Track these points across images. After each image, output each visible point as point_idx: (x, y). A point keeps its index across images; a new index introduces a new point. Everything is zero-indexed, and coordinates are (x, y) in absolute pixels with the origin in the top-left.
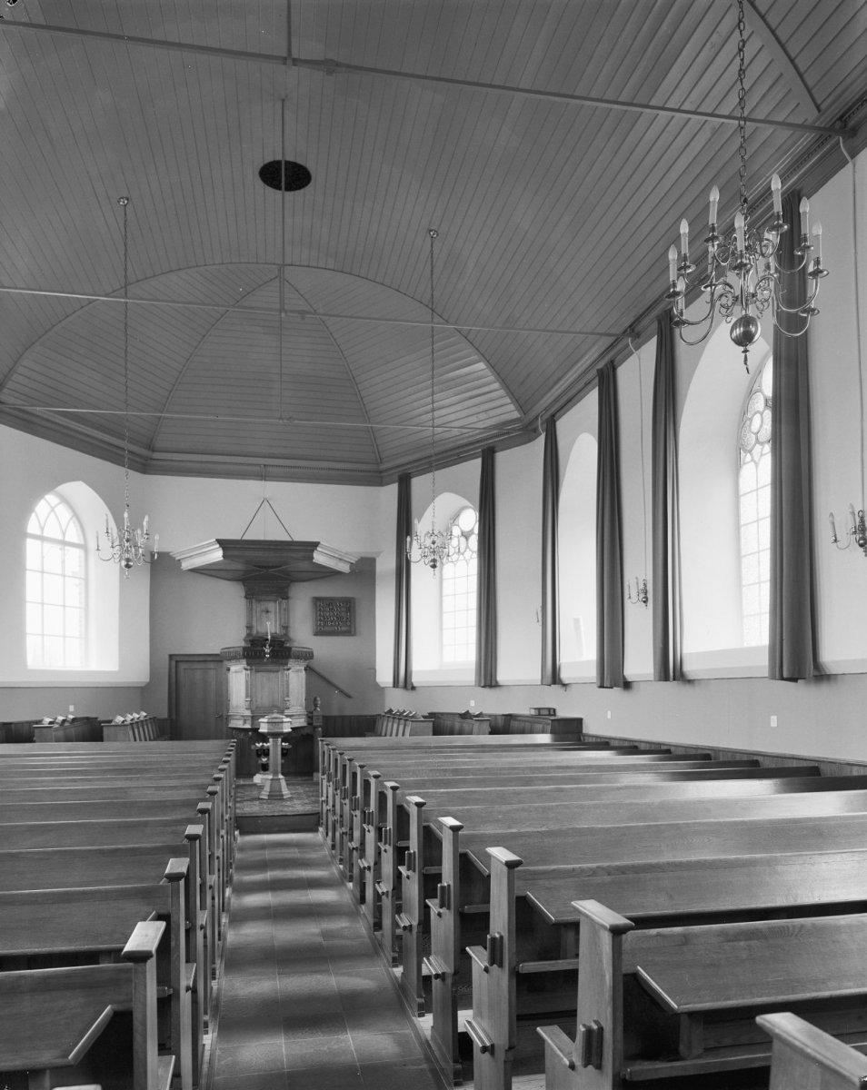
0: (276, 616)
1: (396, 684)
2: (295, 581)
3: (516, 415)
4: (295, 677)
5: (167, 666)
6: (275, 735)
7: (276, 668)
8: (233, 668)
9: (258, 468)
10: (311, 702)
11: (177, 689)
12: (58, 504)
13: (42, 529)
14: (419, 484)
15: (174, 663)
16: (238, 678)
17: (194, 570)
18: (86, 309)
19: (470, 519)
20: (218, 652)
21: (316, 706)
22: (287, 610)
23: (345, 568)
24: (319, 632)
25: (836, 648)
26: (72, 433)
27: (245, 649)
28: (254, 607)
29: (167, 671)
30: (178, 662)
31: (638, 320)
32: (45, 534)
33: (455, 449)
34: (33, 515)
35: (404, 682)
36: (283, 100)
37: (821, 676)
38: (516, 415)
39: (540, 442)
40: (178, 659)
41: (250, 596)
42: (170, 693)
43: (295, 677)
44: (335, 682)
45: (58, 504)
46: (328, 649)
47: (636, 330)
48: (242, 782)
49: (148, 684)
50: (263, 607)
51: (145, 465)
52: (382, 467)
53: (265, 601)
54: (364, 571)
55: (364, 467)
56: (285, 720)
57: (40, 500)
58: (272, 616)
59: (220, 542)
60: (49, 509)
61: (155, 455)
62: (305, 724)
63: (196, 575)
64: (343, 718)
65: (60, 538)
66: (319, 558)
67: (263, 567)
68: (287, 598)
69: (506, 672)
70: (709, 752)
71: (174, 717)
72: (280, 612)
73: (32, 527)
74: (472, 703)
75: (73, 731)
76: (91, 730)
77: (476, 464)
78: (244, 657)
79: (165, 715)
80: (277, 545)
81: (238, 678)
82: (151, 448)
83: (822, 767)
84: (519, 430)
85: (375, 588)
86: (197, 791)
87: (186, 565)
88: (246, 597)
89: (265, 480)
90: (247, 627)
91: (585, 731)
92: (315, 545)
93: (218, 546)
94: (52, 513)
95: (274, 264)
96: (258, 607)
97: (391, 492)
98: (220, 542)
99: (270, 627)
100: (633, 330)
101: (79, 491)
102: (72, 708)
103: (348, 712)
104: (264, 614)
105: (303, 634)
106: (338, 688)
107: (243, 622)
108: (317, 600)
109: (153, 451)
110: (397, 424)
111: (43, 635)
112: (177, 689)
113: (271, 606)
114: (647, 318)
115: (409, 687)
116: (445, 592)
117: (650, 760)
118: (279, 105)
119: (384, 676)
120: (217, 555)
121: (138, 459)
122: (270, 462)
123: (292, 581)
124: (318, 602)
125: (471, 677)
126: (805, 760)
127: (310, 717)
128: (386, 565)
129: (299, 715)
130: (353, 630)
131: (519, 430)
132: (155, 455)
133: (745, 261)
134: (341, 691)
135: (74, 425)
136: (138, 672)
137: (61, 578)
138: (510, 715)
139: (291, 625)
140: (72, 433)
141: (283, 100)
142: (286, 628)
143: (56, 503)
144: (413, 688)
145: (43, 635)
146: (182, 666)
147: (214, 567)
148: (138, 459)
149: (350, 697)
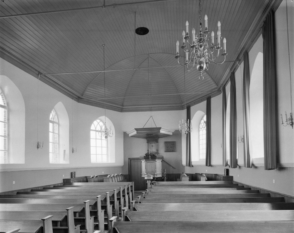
0: (155, 147)
1: (187, 165)
2: (160, 137)
3: (216, 86)
4: (158, 163)
5: (128, 161)
6: (149, 180)
7: (152, 161)
8: (143, 162)
9: (149, 108)
10: (163, 170)
11: (131, 167)
12: (100, 122)
13: (96, 128)
14: (192, 108)
15: (130, 160)
16: (143, 163)
17: (132, 136)
18: (100, 74)
19: (205, 118)
20: (139, 157)
21: (164, 171)
22: (158, 145)
23: (171, 134)
24: (167, 151)
25: (285, 160)
26: (102, 104)
27: (144, 156)
28: (149, 145)
29: (128, 162)
30: (130, 160)
31: (239, 56)
32: (97, 130)
33: (196, 100)
34: (93, 124)
35: (189, 164)
36: (135, 12)
37: (210, 165)
38: (216, 86)
39: (221, 95)
40: (131, 159)
41: (148, 142)
42: (129, 167)
43: (158, 163)
44: (171, 164)
45: (100, 122)
46: (167, 156)
47: (239, 59)
48: (135, 192)
49: (124, 166)
50: (152, 145)
51: (122, 110)
52: (183, 104)
53: (152, 143)
54: (177, 134)
55: (178, 105)
56: (151, 176)
57: (95, 121)
58: (154, 147)
59: (135, 129)
60: (97, 123)
61: (124, 107)
62: (162, 176)
63: (134, 138)
64: (173, 174)
65: (95, 129)
66: (162, 131)
67: (149, 135)
68: (158, 142)
69: (213, 162)
70: (259, 190)
71: (130, 174)
72: (156, 146)
73: (92, 127)
74: (206, 171)
75: (97, 179)
76: (101, 179)
77: (205, 102)
78: (144, 159)
79: (127, 173)
80: (152, 129)
81: (143, 163)
82: (123, 106)
83: (286, 198)
84: (217, 91)
85: (181, 139)
86: (93, 200)
87: (130, 135)
88: (147, 143)
89: (151, 111)
90: (148, 150)
91: (234, 180)
92: (160, 128)
93: (135, 130)
94: (98, 124)
95: (147, 54)
96: (150, 145)
97: (185, 112)
98: (135, 129)
99: (153, 150)
100: (238, 59)
101: (103, 118)
102: (103, 172)
103: (174, 173)
104: (152, 147)
105: (162, 152)
106: (171, 166)
107: (146, 149)
108: (166, 143)
109: (123, 106)
110: (195, 92)
111: (96, 154)
112: (131, 167)
113: (154, 144)
114: (241, 55)
115: (191, 166)
116: (200, 139)
117: (117, 209)
118: (135, 13)
119: (184, 163)
120: (135, 133)
121: (120, 109)
122: (152, 106)
123: (159, 138)
124: (166, 143)
125: (204, 163)
126: (282, 195)
127: (163, 174)
128: (184, 132)
129: (159, 174)
130: (175, 150)
131: (217, 91)
132: (124, 107)
133: (195, 44)
134: (173, 167)
135: (101, 102)
136: (121, 163)
137: (101, 140)
138: (216, 174)
139: (159, 149)
140: (102, 104)
141: (135, 12)
142: (158, 150)
143: (99, 121)
144: (192, 166)
145: (96, 154)
146: (132, 161)
147: (135, 136)
148: (120, 109)
149: (38, 143)
